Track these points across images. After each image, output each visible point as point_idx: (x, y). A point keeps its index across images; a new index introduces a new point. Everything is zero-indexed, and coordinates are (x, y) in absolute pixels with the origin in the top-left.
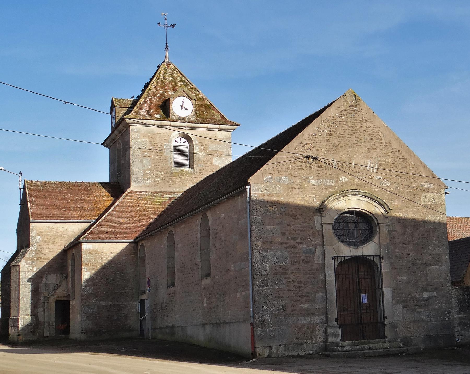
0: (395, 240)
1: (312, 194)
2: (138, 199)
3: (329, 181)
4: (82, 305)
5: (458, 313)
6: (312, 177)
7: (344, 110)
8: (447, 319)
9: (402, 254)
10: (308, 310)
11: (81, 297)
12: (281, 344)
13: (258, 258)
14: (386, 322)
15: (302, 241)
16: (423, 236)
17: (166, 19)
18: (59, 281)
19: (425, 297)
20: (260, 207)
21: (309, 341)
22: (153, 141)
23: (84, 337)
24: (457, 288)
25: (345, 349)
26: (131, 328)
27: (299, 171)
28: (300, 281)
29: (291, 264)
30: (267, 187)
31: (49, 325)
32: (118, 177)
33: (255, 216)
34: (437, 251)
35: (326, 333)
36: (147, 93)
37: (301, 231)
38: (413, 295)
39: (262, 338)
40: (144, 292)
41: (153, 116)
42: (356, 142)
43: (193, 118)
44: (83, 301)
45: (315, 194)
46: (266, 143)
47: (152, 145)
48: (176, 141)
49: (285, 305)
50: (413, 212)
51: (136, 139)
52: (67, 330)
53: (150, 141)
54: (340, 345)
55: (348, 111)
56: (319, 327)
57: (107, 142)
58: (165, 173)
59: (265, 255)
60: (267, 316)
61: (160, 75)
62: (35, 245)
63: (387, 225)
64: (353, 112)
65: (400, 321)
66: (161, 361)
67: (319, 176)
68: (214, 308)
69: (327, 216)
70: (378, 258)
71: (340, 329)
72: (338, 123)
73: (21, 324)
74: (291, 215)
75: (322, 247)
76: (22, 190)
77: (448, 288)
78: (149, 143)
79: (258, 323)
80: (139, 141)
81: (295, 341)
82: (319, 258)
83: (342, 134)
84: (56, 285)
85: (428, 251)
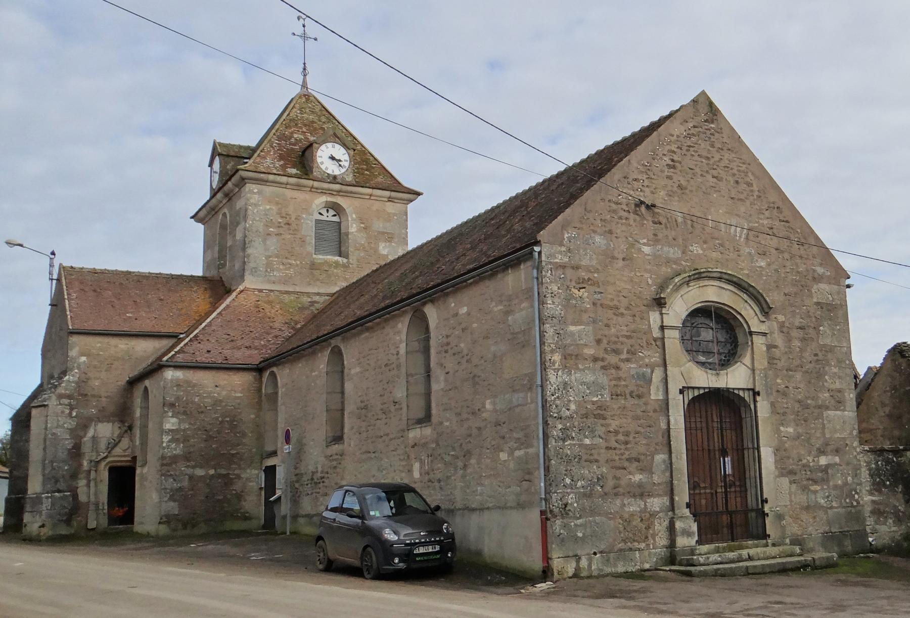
0: (775, 361)
1: (646, 270)
2: (258, 301)
3: (672, 250)
4: (162, 475)
5: (871, 494)
6: (645, 241)
7: (694, 127)
8: (855, 504)
9: (787, 387)
10: (640, 485)
11: (160, 461)
12: (595, 551)
13: (554, 386)
14: (767, 509)
15: (630, 357)
16: (817, 358)
17: (304, 26)
18: (117, 432)
19: (822, 465)
20: (559, 288)
21: (643, 545)
22: (283, 210)
23: (163, 530)
24: (867, 450)
25: (711, 559)
26: (247, 515)
27: (624, 228)
28: (627, 432)
29: (612, 399)
30: (570, 252)
31: (97, 509)
32: (219, 268)
33: (550, 304)
34: (838, 385)
35: (671, 528)
36: (274, 134)
37: (628, 337)
38: (804, 461)
39: (563, 540)
40: (274, 453)
41: (285, 171)
42: (713, 185)
43: (349, 178)
44: (163, 467)
45: (649, 271)
46: (626, 139)
47: (282, 217)
48: (320, 214)
49: (601, 475)
50: (801, 315)
51: (256, 205)
52: (129, 517)
53: (280, 209)
54: (697, 551)
55: (700, 129)
56: (660, 518)
57: (202, 214)
58: (301, 263)
59: (566, 380)
60: (571, 496)
61: (295, 109)
62: (76, 373)
63: (764, 334)
64: (708, 132)
65: (786, 506)
66: (361, 588)
67: (655, 240)
68: (439, 481)
69: (671, 312)
70: (751, 393)
71: (695, 521)
72: (685, 148)
73: (46, 507)
74: (611, 308)
75: (662, 369)
76: (54, 282)
77: (855, 448)
78: (277, 214)
79: (556, 510)
80: (261, 208)
81: (620, 545)
82: (658, 390)
83: (692, 169)
84: (112, 440)
85: (825, 384)
